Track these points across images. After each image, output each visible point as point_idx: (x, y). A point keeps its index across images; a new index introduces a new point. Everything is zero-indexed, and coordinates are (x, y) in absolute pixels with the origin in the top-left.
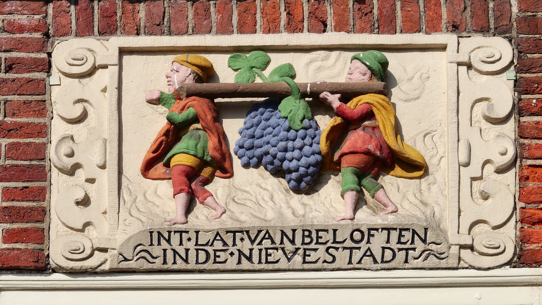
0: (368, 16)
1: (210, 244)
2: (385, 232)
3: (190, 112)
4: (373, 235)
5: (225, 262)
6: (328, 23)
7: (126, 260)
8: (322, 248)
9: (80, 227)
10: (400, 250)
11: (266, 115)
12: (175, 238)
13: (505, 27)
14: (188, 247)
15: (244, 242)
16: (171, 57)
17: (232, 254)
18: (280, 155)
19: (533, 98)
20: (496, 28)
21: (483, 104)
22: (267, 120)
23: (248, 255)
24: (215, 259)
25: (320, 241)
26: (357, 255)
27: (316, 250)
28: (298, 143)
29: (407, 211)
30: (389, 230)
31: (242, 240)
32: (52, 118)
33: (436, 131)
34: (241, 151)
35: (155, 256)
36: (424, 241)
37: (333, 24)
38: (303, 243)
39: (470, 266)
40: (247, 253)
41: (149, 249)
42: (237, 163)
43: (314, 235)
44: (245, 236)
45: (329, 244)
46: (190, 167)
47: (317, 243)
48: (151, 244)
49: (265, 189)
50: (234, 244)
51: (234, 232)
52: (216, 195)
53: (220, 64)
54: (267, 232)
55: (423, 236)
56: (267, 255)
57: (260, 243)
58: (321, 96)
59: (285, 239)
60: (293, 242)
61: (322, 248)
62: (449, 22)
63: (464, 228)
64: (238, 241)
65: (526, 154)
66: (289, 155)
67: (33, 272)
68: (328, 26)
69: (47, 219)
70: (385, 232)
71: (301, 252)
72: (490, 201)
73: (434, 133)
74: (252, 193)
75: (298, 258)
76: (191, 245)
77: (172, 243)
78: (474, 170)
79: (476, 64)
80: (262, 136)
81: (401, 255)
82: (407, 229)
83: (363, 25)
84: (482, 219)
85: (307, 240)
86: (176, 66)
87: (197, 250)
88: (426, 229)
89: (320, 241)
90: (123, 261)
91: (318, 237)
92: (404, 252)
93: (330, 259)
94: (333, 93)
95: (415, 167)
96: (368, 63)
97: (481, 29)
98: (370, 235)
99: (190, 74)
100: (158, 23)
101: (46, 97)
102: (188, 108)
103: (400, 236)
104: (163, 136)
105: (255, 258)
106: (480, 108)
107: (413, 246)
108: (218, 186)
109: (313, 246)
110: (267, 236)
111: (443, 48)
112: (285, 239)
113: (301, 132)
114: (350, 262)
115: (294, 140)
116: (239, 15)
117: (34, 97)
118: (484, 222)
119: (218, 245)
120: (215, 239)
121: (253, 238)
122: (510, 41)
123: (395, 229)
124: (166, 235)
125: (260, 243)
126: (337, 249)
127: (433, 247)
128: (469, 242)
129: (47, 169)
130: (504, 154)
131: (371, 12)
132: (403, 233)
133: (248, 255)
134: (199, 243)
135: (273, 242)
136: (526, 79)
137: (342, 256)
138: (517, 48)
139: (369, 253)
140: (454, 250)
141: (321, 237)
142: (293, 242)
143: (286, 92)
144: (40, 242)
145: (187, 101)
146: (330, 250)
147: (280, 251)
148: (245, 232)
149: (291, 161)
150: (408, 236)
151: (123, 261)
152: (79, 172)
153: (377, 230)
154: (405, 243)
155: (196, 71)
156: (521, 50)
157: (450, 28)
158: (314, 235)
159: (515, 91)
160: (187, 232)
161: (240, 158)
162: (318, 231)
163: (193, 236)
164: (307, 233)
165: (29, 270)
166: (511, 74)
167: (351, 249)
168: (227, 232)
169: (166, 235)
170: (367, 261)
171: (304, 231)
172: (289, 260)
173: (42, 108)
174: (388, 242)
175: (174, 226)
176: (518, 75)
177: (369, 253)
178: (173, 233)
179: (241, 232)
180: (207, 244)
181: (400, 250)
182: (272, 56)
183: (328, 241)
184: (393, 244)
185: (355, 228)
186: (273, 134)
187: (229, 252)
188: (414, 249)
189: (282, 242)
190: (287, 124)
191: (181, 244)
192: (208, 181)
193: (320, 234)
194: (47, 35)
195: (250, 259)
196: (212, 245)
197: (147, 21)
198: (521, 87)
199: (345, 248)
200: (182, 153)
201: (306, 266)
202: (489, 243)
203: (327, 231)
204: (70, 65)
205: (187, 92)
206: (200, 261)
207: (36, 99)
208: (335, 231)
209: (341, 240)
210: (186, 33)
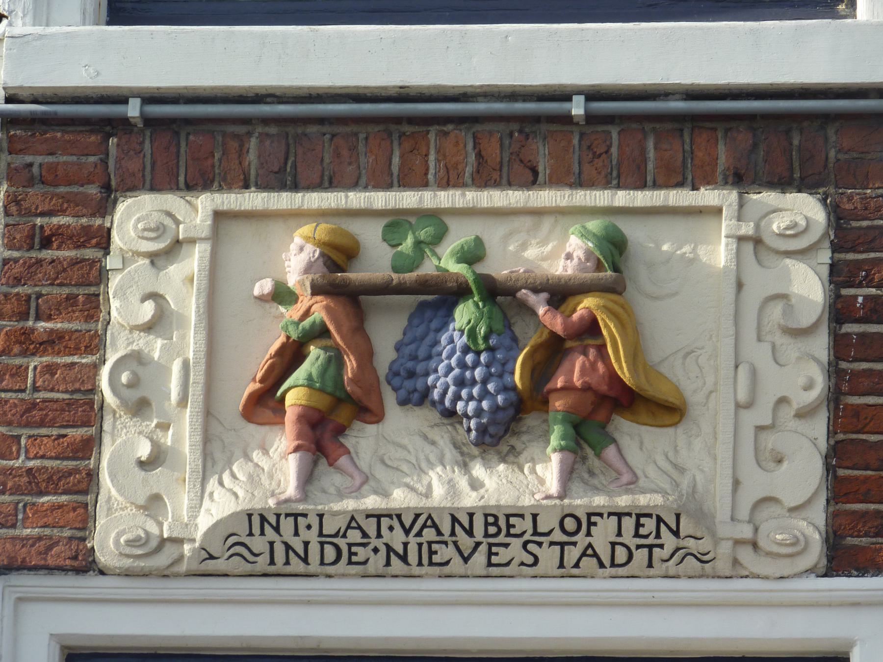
0: (601, 158)
1: (341, 534)
2: (614, 519)
4: (595, 524)
5: (365, 563)
6: (541, 169)
7: (211, 557)
8: (516, 544)
10: (638, 547)
12: (287, 525)
14: (306, 540)
15: (394, 532)
17: (376, 550)
19: (860, 294)
20: (802, 179)
23: (401, 552)
24: (350, 558)
25: (512, 531)
26: (571, 554)
27: (506, 545)
29: (652, 482)
30: (620, 515)
31: (391, 528)
33: (703, 348)
34: (396, 381)
35: (256, 551)
36: (676, 533)
37: (548, 172)
38: (487, 535)
39: (752, 573)
40: (400, 549)
41: (247, 540)
42: (390, 398)
43: (502, 523)
44: (396, 523)
45: (527, 537)
47: (508, 535)
48: (251, 534)
50: (379, 535)
51: (379, 517)
52: (357, 453)
53: (370, 235)
54: (430, 517)
55: (674, 526)
56: (432, 553)
57: (419, 534)
58: (519, 295)
59: (458, 528)
60: (470, 533)
61: (516, 544)
63: (744, 512)
64: (384, 530)
67: (70, 573)
68: (541, 175)
70: (614, 519)
71: (483, 548)
72: (785, 464)
73: (699, 352)
74: (411, 450)
75: (480, 557)
76: (312, 536)
77: (282, 532)
78: (762, 415)
81: (641, 556)
82: (649, 516)
84: (772, 495)
85: (492, 530)
87: (322, 544)
88: (678, 516)
89: (512, 531)
90: (207, 559)
91: (509, 526)
92: (646, 550)
93: (530, 560)
94: (536, 290)
95: (668, 411)
98: (590, 524)
100: (276, 169)
103: (638, 525)
105: (413, 557)
106: (776, 312)
107: (658, 542)
109: (501, 539)
110: (429, 523)
111: (718, 211)
112: (458, 528)
114: (561, 565)
116: (402, 156)
119: (354, 536)
120: (349, 527)
121: (407, 526)
124: (273, 520)
125: (419, 534)
127: (691, 543)
130: (808, 387)
131: (607, 152)
132: (643, 520)
133: (401, 551)
134: (325, 532)
136: (849, 263)
137: (548, 556)
139: (590, 552)
140: (725, 548)
141: (514, 526)
142: (470, 533)
146: (530, 547)
147: (451, 546)
148: (394, 517)
150: (649, 525)
151: (207, 559)
153: (601, 515)
154: (646, 537)
157: (730, 180)
158: (502, 523)
159: (831, 282)
160: (305, 515)
161: (395, 389)
162: (508, 516)
163: (314, 521)
165: (63, 570)
166: (825, 256)
167: (562, 545)
168: (368, 516)
169: (273, 520)
170: (588, 563)
171: (486, 516)
172: (466, 560)
173: (93, 307)
174: (619, 534)
176: (837, 255)
177: (590, 551)
178: (282, 517)
179: (390, 516)
180: (336, 535)
181: (638, 547)
183: (524, 532)
184: (628, 537)
185: (566, 512)
187: (371, 547)
188: (661, 546)
189: (453, 533)
191: (296, 534)
192: (341, 430)
193: (512, 520)
194: (107, 188)
195: (404, 558)
196: (344, 536)
197: (261, 165)
198: (839, 276)
199: (552, 544)
201: (494, 570)
203: (522, 516)
206: (326, 561)
208: (535, 516)
209: (546, 530)
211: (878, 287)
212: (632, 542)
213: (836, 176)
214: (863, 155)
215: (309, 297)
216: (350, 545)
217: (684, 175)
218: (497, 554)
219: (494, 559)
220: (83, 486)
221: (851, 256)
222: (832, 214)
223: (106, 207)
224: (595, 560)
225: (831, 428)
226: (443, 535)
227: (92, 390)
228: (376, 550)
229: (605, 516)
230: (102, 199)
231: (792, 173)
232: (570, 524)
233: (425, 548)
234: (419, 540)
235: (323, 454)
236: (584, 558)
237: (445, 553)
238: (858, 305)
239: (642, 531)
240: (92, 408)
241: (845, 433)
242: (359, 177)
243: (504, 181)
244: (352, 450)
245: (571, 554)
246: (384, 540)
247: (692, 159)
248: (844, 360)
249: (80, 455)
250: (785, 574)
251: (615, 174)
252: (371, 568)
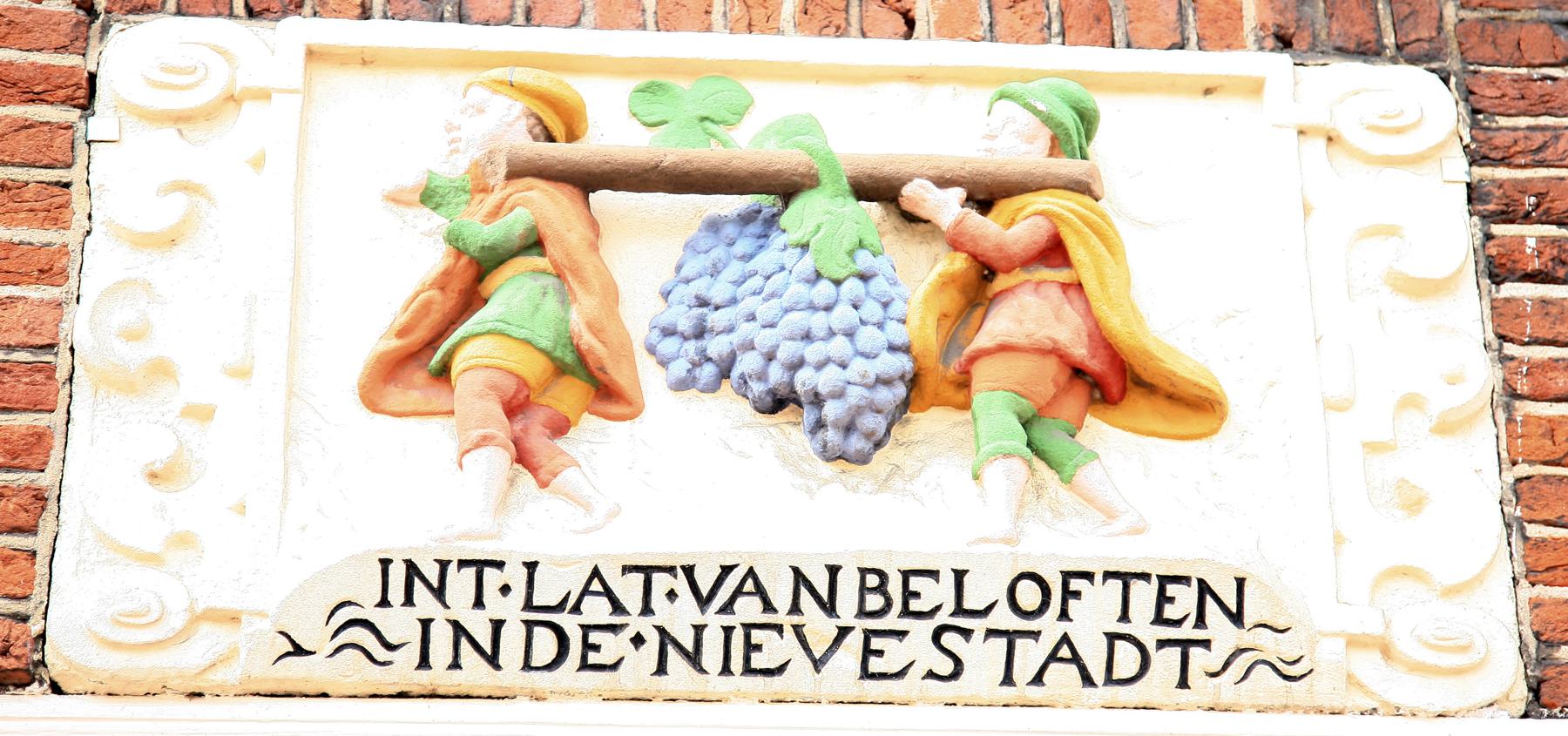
2: (1117, 585)
3: (515, 224)
4: (1077, 594)
7: (298, 651)
8: (921, 631)
9: (152, 545)
10: (1162, 644)
11: (743, 246)
12: (461, 584)
13: (1426, 46)
16: (460, 78)
17: (638, 640)
18: (787, 351)
20: (1399, 47)
22: (747, 258)
23: (689, 645)
24: (584, 657)
25: (914, 605)
26: (1030, 656)
27: (901, 634)
28: (843, 315)
30: (1125, 578)
32: (89, 233)
34: (669, 346)
35: (393, 640)
36: (1237, 618)
37: (933, 18)
38: (863, 613)
39: (1386, 704)
41: (377, 616)
43: (895, 588)
44: (681, 585)
47: (906, 612)
48: (384, 602)
50: (647, 610)
51: (648, 571)
54: (751, 572)
56: (751, 647)
57: (727, 608)
60: (829, 607)
61: (921, 631)
62: (1263, 27)
65: (1523, 386)
66: (813, 352)
69: (46, 525)
71: (854, 641)
76: (511, 610)
79: (1352, 133)
80: (733, 301)
82: (1183, 580)
83: (1018, 25)
85: (874, 602)
86: (478, 94)
87: (530, 625)
88: (1241, 583)
89: (914, 605)
90: (288, 654)
91: (909, 594)
92: (1177, 651)
93: (946, 667)
94: (943, 182)
96: (1041, 107)
97: (1359, 45)
98: (1068, 594)
99: (518, 118)
101: (75, 175)
102: (512, 209)
103: (1163, 599)
104: (431, 287)
105: (712, 656)
107: (1200, 634)
108: (595, 441)
110: (749, 586)
111: (1255, 88)
113: (853, 287)
114: (1008, 680)
115: (828, 309)
117: (34, 171)
119: (597, 610)
120: (586, 591)
121: (705, 592)
122: (1446, 81)
123: (1145, 576)
125: (727, 608)
126: (966, 633)
128: (1374, 627)
129: (61, 374)
132: (1171, 590)
134: (536, 602)
135: (768, 607)
137: (983, 657)
138: (1466, 100)
141: (917, 595)
142: (829, 607)
143: (803, 175)
144: (18, 591)
145: (509, 190)
146: (949, 639)
149: (820, 366)
150: (1184, 600)
151: (288, 654)
153: (1088, 576)
154: (1178, 623)
155: (535, 110)
156: (1478, 106)
157: (1270, 42)
158: (895, 588)
160: (500, 565)
161: (664, 363)
162: (906, 575)
163: (516, 576)
164: (872, 581)
167: (1011, 636)
168: (627, 569)
169: (433, 576)
170: (1063, 676)
171: (864, 572)
172: (818, 664)
174: (1124, 617)
175: (459, 544)
176: (1475, 169)
177: (1066, 652)
178: (452, 568)
179: (671, 570)
181: (1162, 644)
182: (761, 91)
183: (938, 608)
186: (767, 291)
187: (630, 633)
188: (1206, 644)
189: (795, 609)
190: (807, 264)
191: (479, 603)
192: (560, 427)
193: (915, 583)
195: (694, 658)
196: (576, 609)
199: (991, 633)
200: (489, 333)
202: (1440, 633)
203: (933, 574)
205: (510, 163)
207: (40, 178)
208: (959, 575)
210: (508, 21)
211: (1560, 224)
212: (1150, 635)
213: (1460, 44)
214: (1507, 14)
215: (501, 183)
216: (586, 629)
217: (1182, 33)
218: (880, 653)
219: (875, 665)
220: (23, 519)
221: (1502, 173)
222: (1462, 104)
223: (87, 39)
224: (1073, 668)
225: (1504, 455)
226: (775, 611)
227: (51, 346)
228: (638, 640)
229: (1098, 578)
230: (78, 23)
231: (1381, 37)
232: (1029, 595)
233: (738, 638)
234: (727, 620)
235: (526, 467)
236: (1053, 666)
237: (774, 649)
238: (1529, 251)
239: (1170, 612)
240: (51, 377)
241: (1531, 463)
242: (582, 12)
243: (854, 28)
244: (582, 462)
245: (1030, 656)
246: (657, 620)
247: (1195, 10)
248: (1512, 341)
249: (27, 460)
250: (1453, 708)
251: (1056, 27)
252: (624, 679)
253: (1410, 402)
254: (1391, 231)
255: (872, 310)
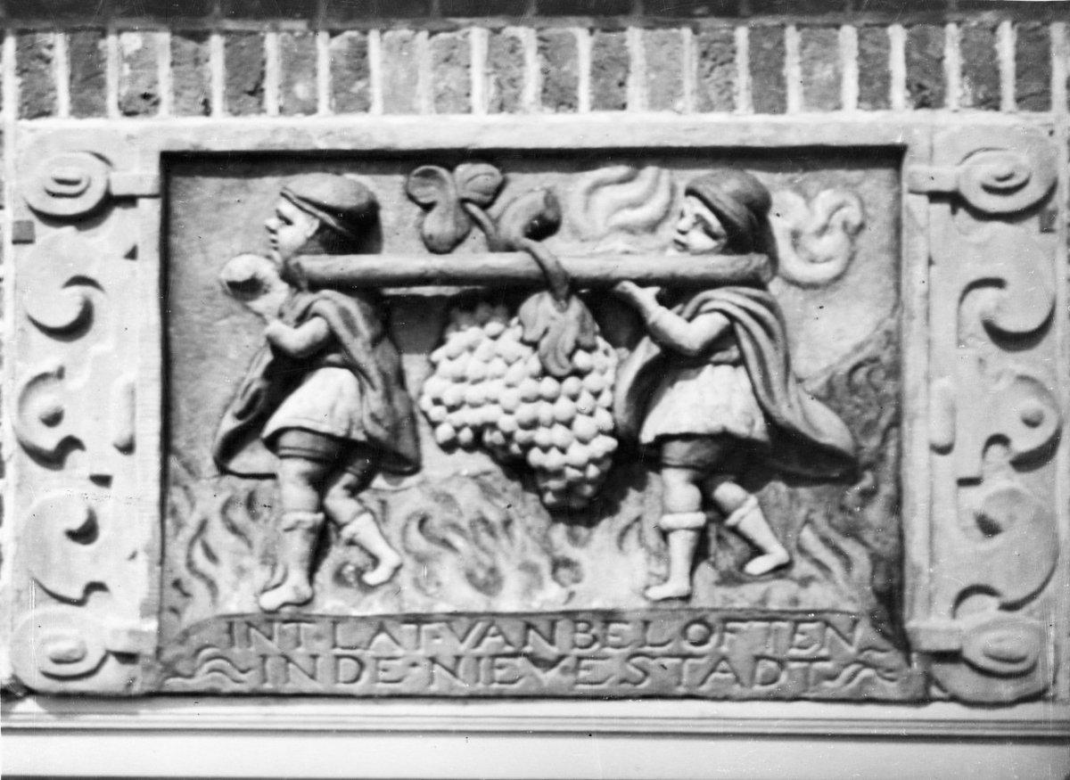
9: (76, 593)
21: (989, 293)
28: (564, 408)
46: (330, 437)
49: (569, 257)
58: (619, 288)
66: (541, 435)
115: (552, 400)
118: (988, 591)
149: (545, 449)
152: (74, 456)
204: (54, 195)
253: (999, 440)
254: (998, 283)
255: (586, 401)
